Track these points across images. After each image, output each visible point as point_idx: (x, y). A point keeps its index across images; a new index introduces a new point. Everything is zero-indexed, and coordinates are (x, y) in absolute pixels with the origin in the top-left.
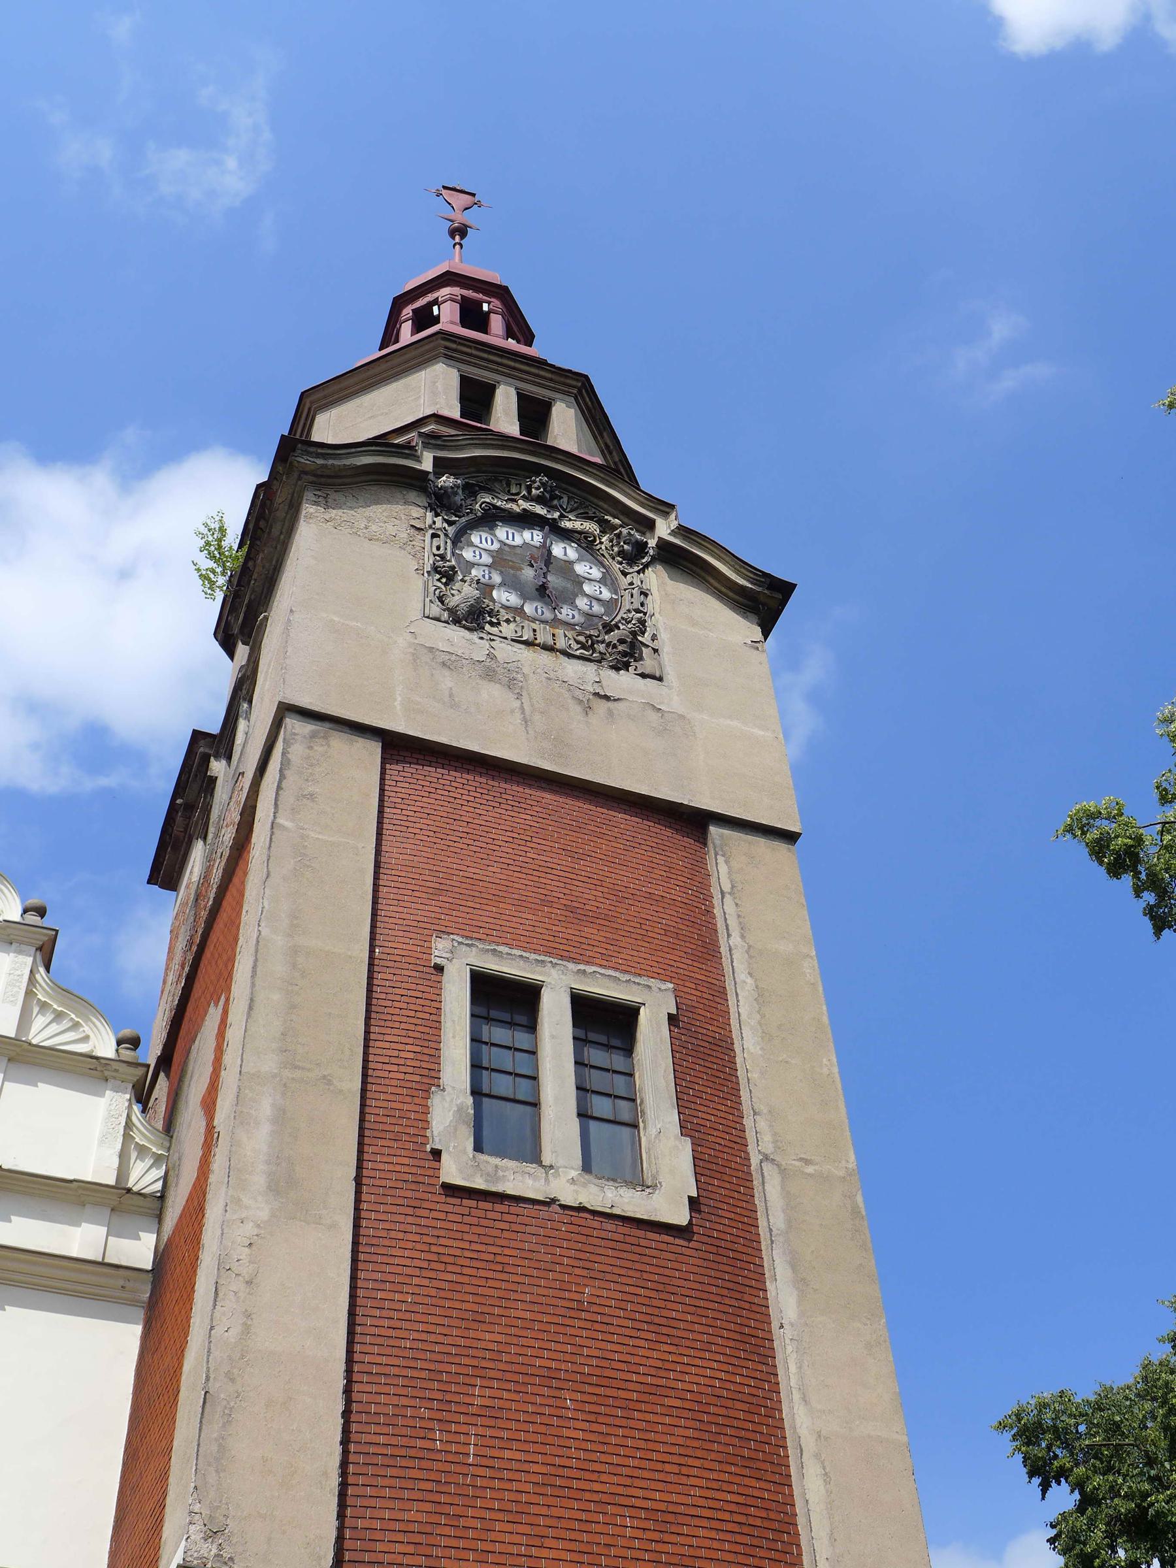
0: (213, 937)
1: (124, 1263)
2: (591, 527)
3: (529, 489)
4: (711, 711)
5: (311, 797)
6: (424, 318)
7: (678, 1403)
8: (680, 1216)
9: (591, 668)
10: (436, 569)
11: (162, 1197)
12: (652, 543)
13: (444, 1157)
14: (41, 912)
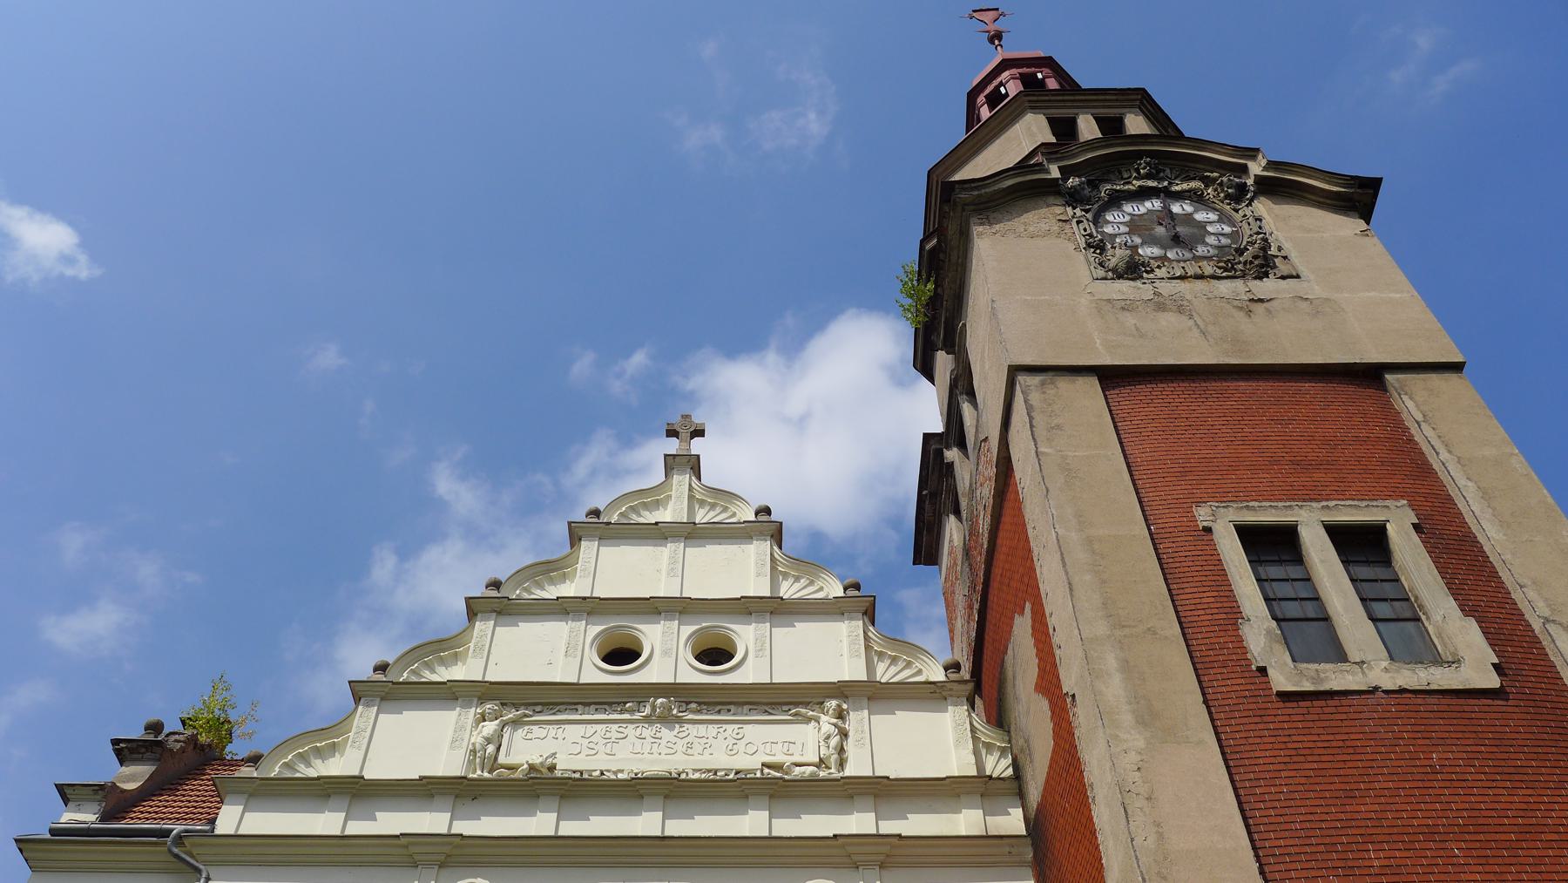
0: (996, 571)
1: (1003, 833)
2: (1194, 184)
3: (1137, 171)
4: (1342, 291)
5: (1058, 427)
6: (995, 99)
7: (1556, 837)
8: (1493, 681)
9: (1239, 283)
10: (1089, 245)
11: (1018, 776)
12: (1250, 182)
13: (1270, 672)
14: (857, 587)
